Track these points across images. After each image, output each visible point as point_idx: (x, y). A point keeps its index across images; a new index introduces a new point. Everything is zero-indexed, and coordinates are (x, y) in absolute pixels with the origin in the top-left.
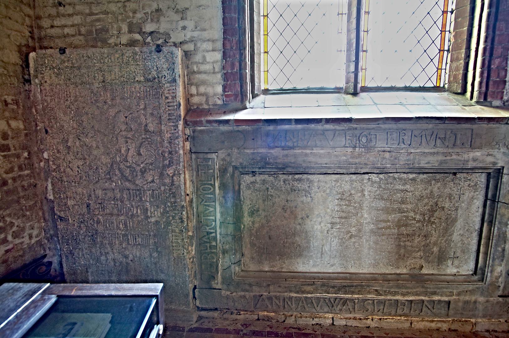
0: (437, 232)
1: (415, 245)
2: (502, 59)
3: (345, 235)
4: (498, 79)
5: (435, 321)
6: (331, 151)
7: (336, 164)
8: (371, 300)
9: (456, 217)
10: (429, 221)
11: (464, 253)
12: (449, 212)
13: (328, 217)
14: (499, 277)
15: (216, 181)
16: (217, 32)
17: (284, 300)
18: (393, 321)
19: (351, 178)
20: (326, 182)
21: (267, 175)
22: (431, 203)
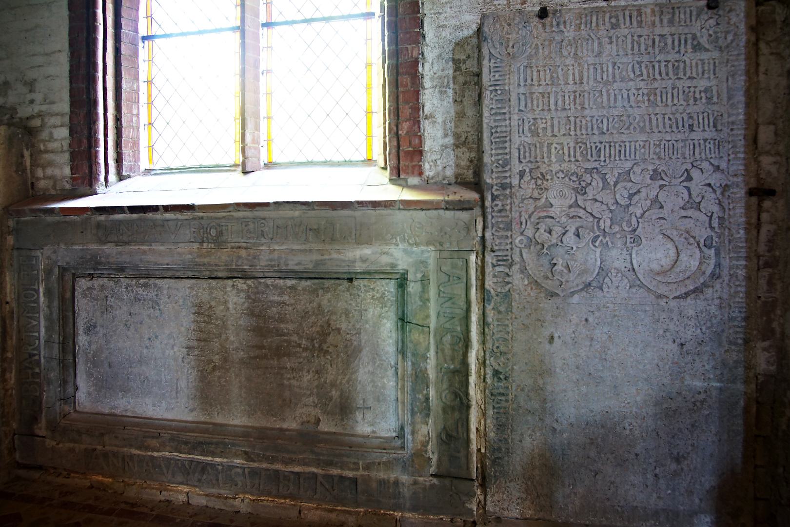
0: (335, 366)
1: (305, 385)
2: (412, 122)
3: (205, 366)
4: (410, 149)
5: (337, 510)
6: (173, 247)
7: (179, 265)
8: (241, 468)
9: (360, 345)
10: (321, 349)
11: (379, 401)
12: (348, 336)
13: (182, 339)
14: (428, 442)
15: (41, 286)
16: (64, 106)
17: (123, 459)
18: (272, 504)
19: (209, 284)
20: (177, 289)
21: (107, 279)
22: (320, 323)
